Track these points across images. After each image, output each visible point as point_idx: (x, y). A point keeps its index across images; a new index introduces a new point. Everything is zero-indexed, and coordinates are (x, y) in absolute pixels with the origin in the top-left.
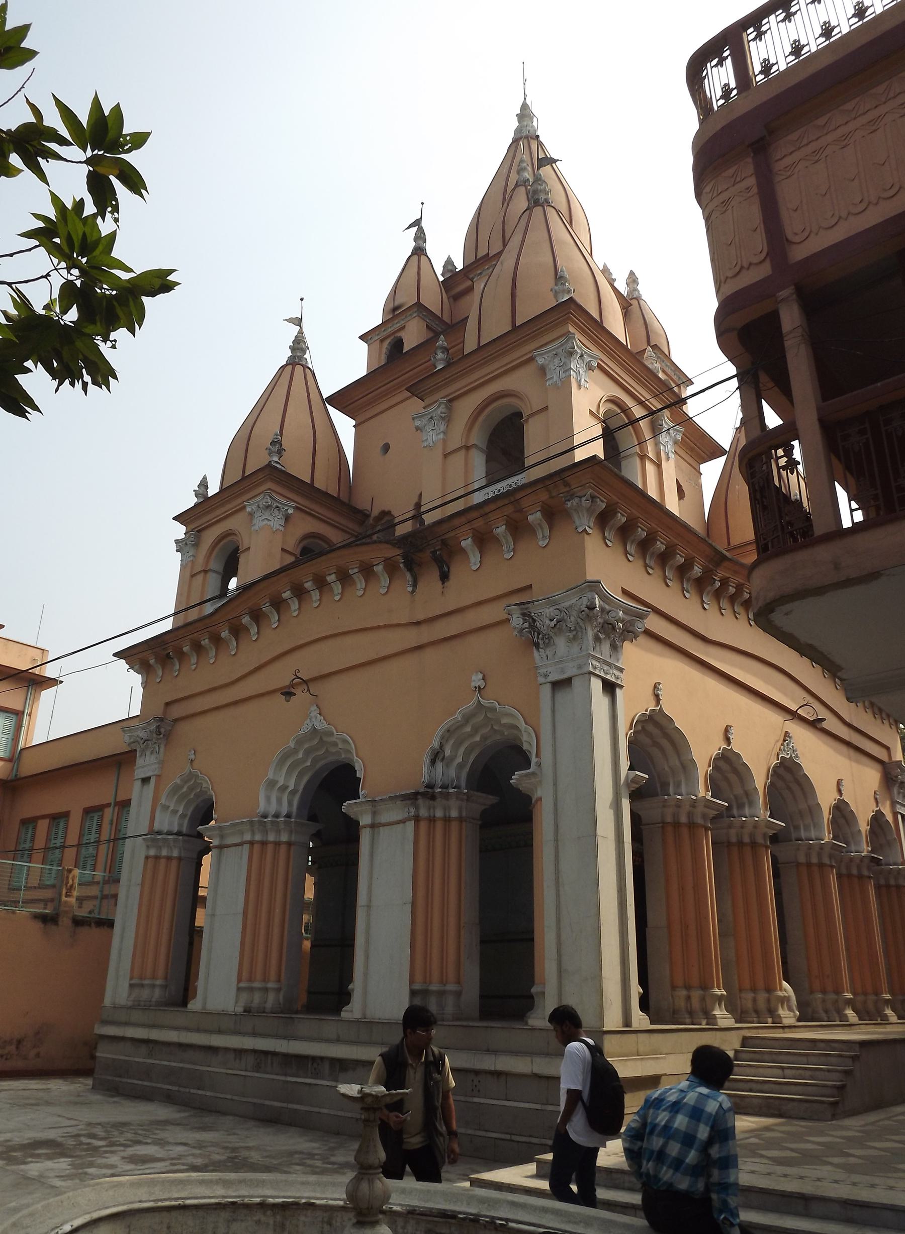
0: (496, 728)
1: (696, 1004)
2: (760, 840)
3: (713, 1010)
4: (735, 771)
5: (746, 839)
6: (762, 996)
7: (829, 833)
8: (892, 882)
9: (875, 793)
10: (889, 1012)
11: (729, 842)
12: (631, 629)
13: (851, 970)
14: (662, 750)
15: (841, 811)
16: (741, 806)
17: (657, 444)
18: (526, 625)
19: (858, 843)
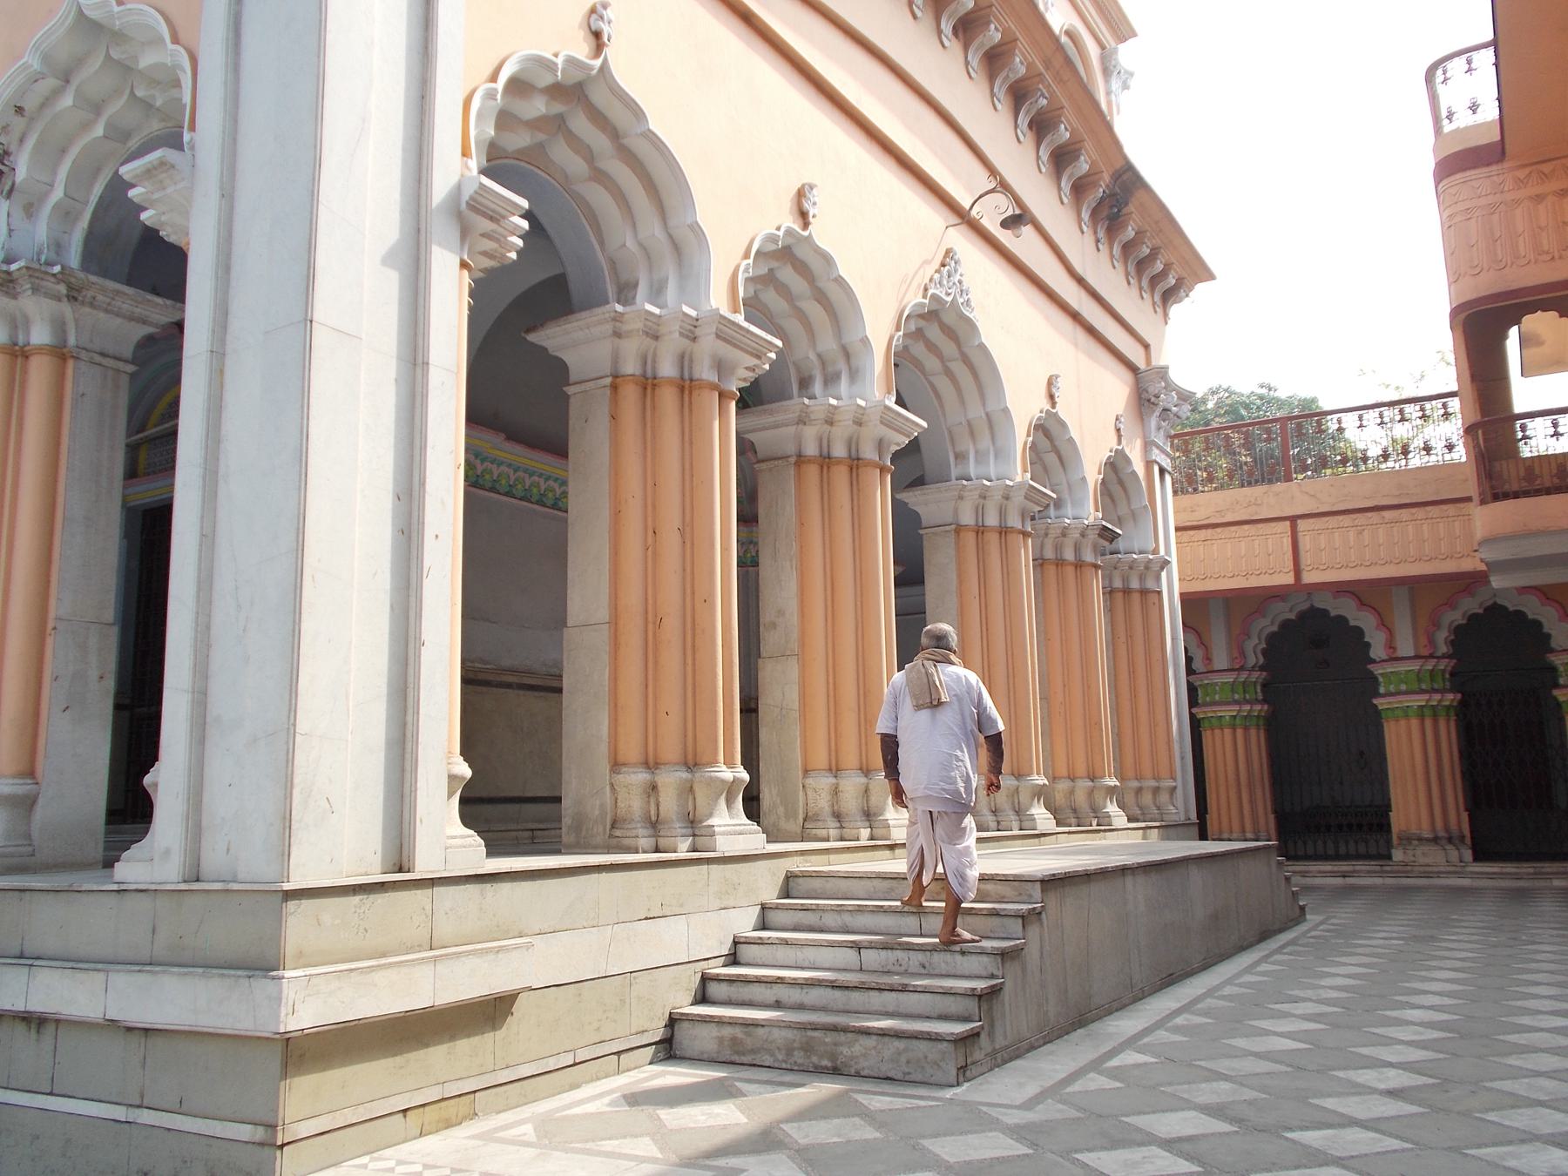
0: (140, 93)
1: (669, 803)
2: (869, 453)
3: (710, 815)
4: (821, 298)
5: (839, 451)
7: (1025, 471)
8: (1135, 584)
10: (1112, 809)
11: (799, 456)
13: (1048, 734)
15: (1050, 439)
16: (831, 380)
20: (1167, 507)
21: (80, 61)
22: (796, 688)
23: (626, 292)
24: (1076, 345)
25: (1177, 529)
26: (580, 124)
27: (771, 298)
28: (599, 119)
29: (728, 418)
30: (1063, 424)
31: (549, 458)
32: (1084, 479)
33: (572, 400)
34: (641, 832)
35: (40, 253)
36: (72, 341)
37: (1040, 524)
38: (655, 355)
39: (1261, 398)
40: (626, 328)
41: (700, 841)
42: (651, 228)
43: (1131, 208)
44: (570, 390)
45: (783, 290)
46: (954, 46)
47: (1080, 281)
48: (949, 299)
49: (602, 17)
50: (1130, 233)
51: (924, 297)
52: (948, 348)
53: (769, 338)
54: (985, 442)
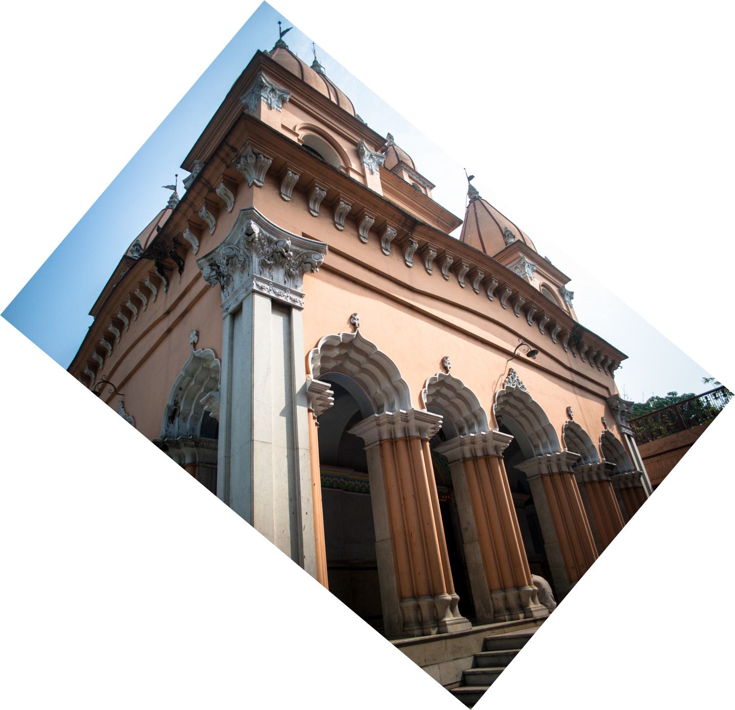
0: (213, 376)
1: (426, 612)
2: (492, 452)
3: (444, 616)
4: (460, 396)
5: (480, 454)
6: (512, 594)
8: (630, 485)
9: (602, 419)
12: (308, 260)
14: (373, 376)
15: (573, 432)
16: (471, 427)
17: (361, 164)
18: (214, 273)
19: (594, 456)
20: (635, 451)
21: (196, 370)
22: (480, 554)
23: (380, 409)
24: (575, 393)
25: (643, 459)
26: (353, 355)
27: (440, 400)
28: (360, 351)
29: (426, 449)
30: (578, 426)
31: (361, 474)
32: (593, 446)
33: (367, 453)
34: (415, 627)
35: (188, 433)
36: (197, 460)
37: (579, 468)
38: (394, 430)
39: (671, 398)
40: (381, 422)
41: (442, 629)
42: (386, 384)
43: (583, 339)
44: (366, 449)
45: (445, 397)
46: (496, 300)
47: (570, 370)
48: (515, 387)
49: (355, 319)
50: (586, 348)
51: (504, 388)
52: (520, 405)
53: (437, 415)
54: (545, 439)
